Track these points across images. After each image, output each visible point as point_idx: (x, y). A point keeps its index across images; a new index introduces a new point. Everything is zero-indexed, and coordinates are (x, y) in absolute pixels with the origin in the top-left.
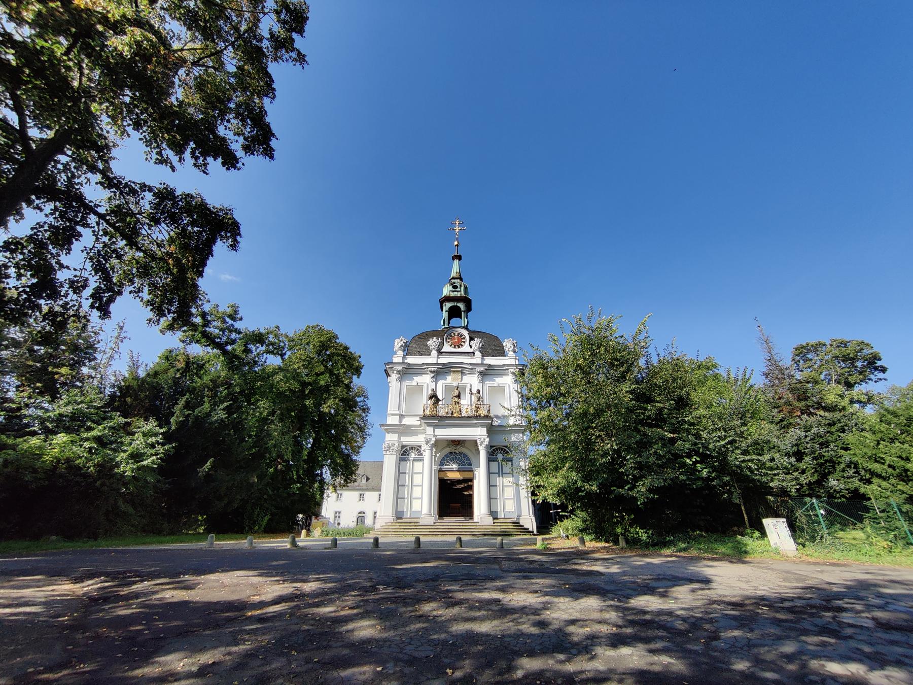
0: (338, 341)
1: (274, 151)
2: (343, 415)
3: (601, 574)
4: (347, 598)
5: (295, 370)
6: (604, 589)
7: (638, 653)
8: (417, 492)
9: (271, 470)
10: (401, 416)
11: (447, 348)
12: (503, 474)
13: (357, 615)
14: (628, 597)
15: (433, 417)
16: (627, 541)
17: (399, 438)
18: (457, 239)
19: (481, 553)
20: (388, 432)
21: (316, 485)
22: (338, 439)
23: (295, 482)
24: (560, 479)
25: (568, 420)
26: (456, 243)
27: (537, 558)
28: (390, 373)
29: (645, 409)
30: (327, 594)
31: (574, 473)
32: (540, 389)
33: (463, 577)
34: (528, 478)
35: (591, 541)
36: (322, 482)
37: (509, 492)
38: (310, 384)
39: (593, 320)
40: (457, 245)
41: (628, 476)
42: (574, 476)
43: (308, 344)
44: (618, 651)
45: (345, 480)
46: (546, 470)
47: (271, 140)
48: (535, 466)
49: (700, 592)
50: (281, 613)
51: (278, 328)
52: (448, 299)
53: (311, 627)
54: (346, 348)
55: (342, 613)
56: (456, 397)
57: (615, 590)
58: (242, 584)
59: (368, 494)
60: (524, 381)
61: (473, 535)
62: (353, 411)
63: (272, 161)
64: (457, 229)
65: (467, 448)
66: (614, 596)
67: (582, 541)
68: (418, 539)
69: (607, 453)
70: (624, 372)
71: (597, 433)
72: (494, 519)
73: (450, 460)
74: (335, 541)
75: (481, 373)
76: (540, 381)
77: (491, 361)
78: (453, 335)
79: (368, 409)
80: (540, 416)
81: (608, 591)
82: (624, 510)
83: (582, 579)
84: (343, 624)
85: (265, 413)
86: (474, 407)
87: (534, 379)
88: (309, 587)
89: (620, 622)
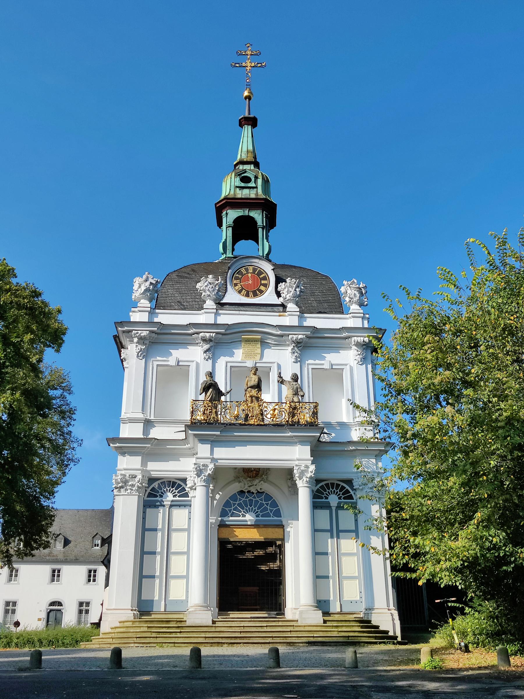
0: (14, 281)
10: (148, 424)
15: (208, 424)
17: (144, 463)
19: (321, 677)
20: (123, 454)
26: (246, 93)
28: (125, 340)
40: (249, 98)
45: (27, 544)
54: (36, 294)
59: (67, 570)
62: (45, 416)
67: (505, 656)
68: (196, 653)
74: (37, 657)
75: (298, 344)
78: (243, 270)
79: (72, 412)
86: (286, 407)
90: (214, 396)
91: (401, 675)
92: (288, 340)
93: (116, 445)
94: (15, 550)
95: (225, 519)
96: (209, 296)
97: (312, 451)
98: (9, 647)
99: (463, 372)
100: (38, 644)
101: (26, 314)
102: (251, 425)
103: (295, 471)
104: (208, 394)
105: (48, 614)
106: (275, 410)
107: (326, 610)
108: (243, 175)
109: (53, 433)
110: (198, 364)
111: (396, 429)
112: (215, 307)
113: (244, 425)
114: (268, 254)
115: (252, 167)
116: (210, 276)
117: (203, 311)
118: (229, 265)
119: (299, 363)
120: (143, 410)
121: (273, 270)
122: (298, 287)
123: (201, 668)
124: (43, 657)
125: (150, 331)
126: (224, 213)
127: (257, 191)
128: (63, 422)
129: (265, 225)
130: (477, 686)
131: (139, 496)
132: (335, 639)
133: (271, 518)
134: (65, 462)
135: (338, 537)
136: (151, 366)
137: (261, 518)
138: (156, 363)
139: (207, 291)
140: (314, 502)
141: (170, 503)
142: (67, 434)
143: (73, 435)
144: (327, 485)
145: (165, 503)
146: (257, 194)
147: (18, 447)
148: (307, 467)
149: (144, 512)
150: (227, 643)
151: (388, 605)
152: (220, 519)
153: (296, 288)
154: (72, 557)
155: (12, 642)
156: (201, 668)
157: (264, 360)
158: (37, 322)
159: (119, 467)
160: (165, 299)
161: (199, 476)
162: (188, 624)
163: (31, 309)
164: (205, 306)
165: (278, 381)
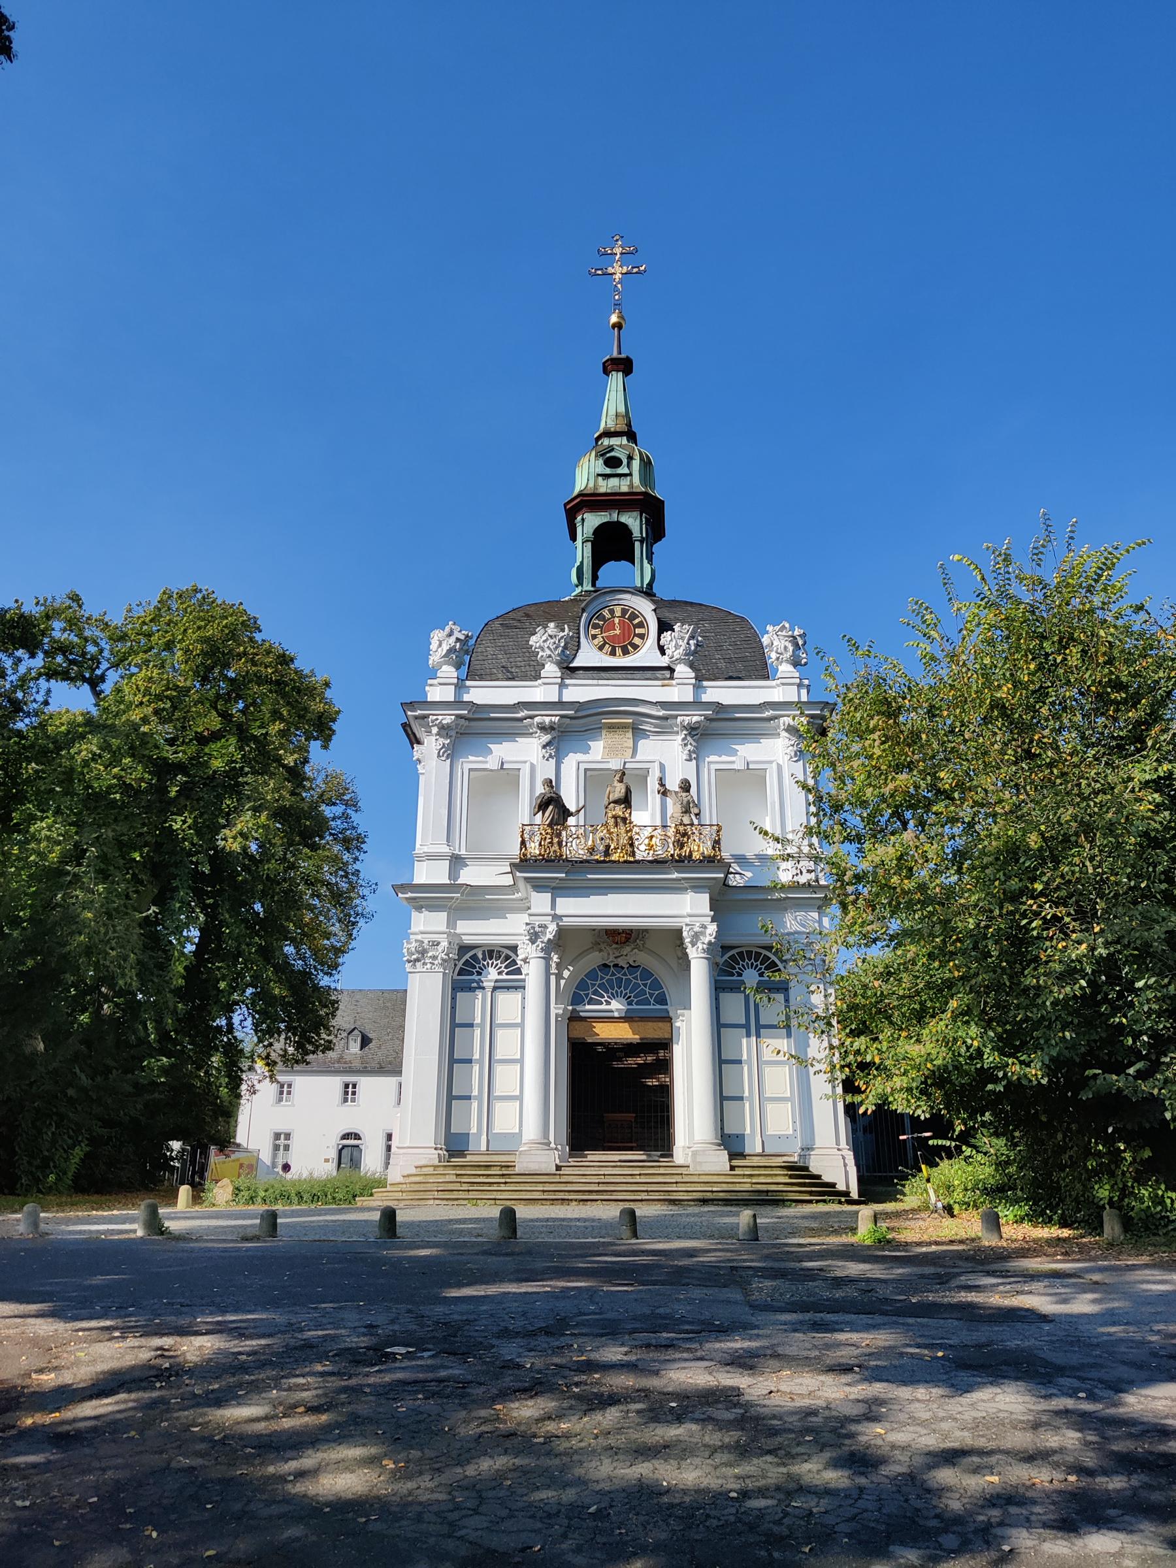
0: (258, 637)
1: (11, 28)
2: (284, 859)
3: (1044, 1318)
4: (301, 1380)
5: (135, 727)
6: (1046, 1364)
7: (1138, 1550)
9: (84, 1018)
10: (457, 862)
11: (589, 655)
12: (759, 1027)
13: (327, 1429)
14: (1119, 1387)
16: (1127, 1224)
17: (451, 923)
18: (617, 305)
19: (690, 1253)
20: (419, 909)
21: (216, 1060)
22: (272, 928)
23: (152, 1053)
24: (929, 1047)
25: (959, 871)
26: (614, 319)
27: (854, 1269)
28: (420, 732)
30: (243, 1368)
31: (974, 1030)
32: (875, 774)
33: (638, 1325)
34: (836, 1042)
35: (1020, 1221)
36: (233, 1052)
38: (180, 768)
39: (1048, 559)
40: (618, 326)
41: (1136, 1036)
42: (973, 1033)
43: (169, 646)
44: (1079, 1542)
45: (299, 1046)
46: (888, 1018)
48: (853, 1007)
50: (115, 1422)
51: (75, 598)
53: (199, 1461)
54: (285, 660)
55: (287, 1423)
56: (616, 802)
57: (1082, 1367)
58: (8, 1337)
59: (366, 1083)
60: (825, 755)
61: (673, 1202)
62: (314, 847)
64: (618, 271)
65: (652, 952)
66: (1076, 1383)
67: (993, 1222)
68: (509, 1216)
70: (1138, 723)
71: (1049, 911)
72: (732, 1156)
73: (601, 986)
75: (692, 730)
76: (877, 752)
78: (606, 613)
79: (360, 839)
80: (872, 857)
81: (1061, 1370)
82: (1121, 1134)
83: (984, 1333)
84: (289, 1454)
85: (53, 857)
86: (671, 832)
87: (856, 747)
89: (1090, 1460)
90: (556, 817)
91: (819, 1251)
92: (677, 726)
94: (280, 1055)
95: (579, 1008)
96: (550, 656)
97: (711, 899)
98: (253, 1203)
99: (341, 905)
101: (271, 692)
102: (614, 862)
103: (685, 934)
104: (547, 814)
105: (340, 1152)
106: (652, 837)
107: (739, 1150)
108: (608, 455)
109: (331, 874)
110: (533, 767)
111: (827, 868)
112: (559, 674)
113: (604, 862)
114: (650, 584)
115: (624, 440)
116: (552, 625)
117: (540, 681)
118: (583, 605)
119: (694, 761)
120: (448, 840)
121: (655, 610)
122: (692, 637)
123: (516, 1238)
124: (279, 1221)
125: (457, 716)
126: (579, 518)
127: (631, 481)
128: (346, 857)
129: (644, 535)
130: (987, 1268)
131: (444, 974)
132: (746, 1196)
133: (652, 1007)
134: (352, 919)
135: (758, 1036)
136: (460, 770)
137: (635, 1007)
138: (467, 767)
139: (547, 650)
140: (716, 981)
141: (492, 984)
142: (353, 874)
143: (362, 875)
144: (741, 954)
145: (485, 984)
147: (273, 897)
148: (704, 927)
149: (454, 999)
150: (576, 1200)
151: (838, 1143)
152: (570, 1008)
153: (689, 640)
156: (516, 1238)
157: (638, 757)
158: (288, 704)
159: (413, 929)
160: (482, 663)
161: (533, 943)
162: (517, 1170)
163: (278, 683)
165: (659, 792)
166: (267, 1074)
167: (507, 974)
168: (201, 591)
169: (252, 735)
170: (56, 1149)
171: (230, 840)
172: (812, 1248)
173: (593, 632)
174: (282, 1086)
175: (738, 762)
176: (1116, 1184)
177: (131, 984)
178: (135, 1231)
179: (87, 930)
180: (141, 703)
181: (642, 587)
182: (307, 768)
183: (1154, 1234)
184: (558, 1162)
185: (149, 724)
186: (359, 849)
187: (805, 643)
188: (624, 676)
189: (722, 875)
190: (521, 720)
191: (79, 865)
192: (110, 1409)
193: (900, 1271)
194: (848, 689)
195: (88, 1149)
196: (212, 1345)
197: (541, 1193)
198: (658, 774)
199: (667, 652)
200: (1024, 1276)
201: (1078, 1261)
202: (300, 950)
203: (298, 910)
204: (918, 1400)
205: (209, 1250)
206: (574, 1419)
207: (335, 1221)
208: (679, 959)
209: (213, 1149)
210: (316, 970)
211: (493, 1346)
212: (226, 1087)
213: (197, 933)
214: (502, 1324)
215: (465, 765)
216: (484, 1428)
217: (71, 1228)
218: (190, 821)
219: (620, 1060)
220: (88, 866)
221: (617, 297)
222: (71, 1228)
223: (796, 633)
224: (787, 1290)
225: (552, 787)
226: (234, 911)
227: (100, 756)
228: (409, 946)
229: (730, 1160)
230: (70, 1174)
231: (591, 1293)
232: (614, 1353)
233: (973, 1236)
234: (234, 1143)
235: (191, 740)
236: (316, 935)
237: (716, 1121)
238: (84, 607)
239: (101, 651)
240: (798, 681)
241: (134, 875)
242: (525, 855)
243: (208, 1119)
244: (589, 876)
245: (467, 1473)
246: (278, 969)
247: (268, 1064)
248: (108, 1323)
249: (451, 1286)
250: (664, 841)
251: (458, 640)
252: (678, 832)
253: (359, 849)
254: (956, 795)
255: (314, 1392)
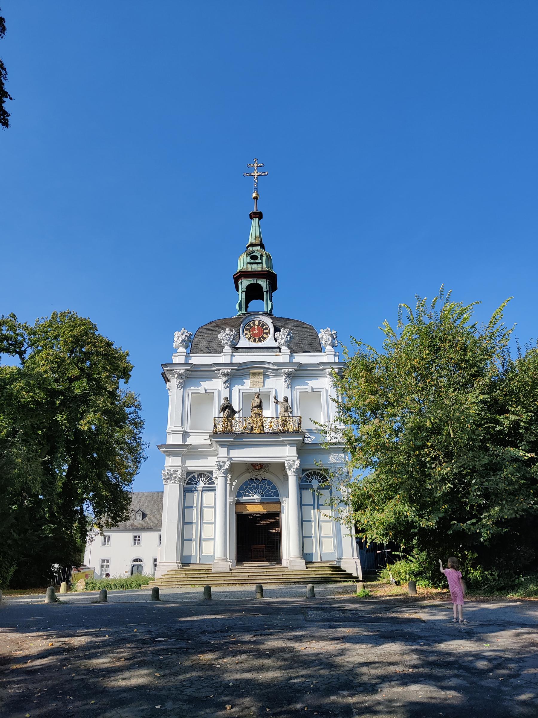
0: (96, 333)
1: (8, 116)
2: (108, 433)
3: (424, 622)
5: (41, 375)
8: (208, 531)
10: (186, 434)
11: (244, 342)
15: (226, 434)
17: (183, 462)
20: (169, 456)
21: (75, 525)
26: (254, 195)
28: (169, 377)
29: (497, 422)
30: (98, 647)
32: (362, 396)
33: (258, 628)
36: (83, 522)
37: (328, 528)
38: (61, 393)
40: (256, 198)
43: (56, 337)
45: (114, 518)
47: (4, 102)
49: (525, 636)
50: (50, 666)
51: (13, 316)
52: (244, 275)
53: (84, 677)
54: (109, 345)
55: (117, 664)
59: (144, 535)
62: (121, 427)
63: (6, 129)
64: (256, 174)
65: (272, 473)
67: (413, 586)
68: (208, 589)
69: (446, 479)
71: (433, 454)
72: (307, 563)
73: (250, 489)
75: (289, 375)
77: (302, 358)
78: (251, 324)
79: (142, 423)
82: (465, 548)
87: (355, 384)
88: (78, 641)
93: (163, 450)
94: (105, 523)
95: (240, 499)
97: (297, 449)
100: (113, 587)
102: (255, 433)
103: (286, 465)
105: (132, 568)
106: (271, 422)
107: (309, 560)
108: (252, 254)
109: (128, 439)
110: (219, 391)
112: (231, 351)
113: (250, 433)
114: (271, 310)
115: (259, 248)
116: (227, 329)
117: (222, 354)
118: (241, 321)
119: (290, 388)
121: (272, 322)
122: (288, 334)
125: (186, 370)
126: (240, 282)
127: (262, 266)
128: (135, 431)
130: (408, 604)
131: (180, 484)
133: (272, 497)
137: (265, 497)
138: (190, 392)
140: (300, 485)
142: (138, 439)
143: (142, 440)
145: (198, 489)
146: (262, 268)
147: (102, 450)
149: (184, 495)
151: (353, 556)
152: (236, 499)
153: (287, 336)
154: (148, 527)
155: (96, 587)
157: (265, 387)
158: (110, 364)
159: (166, 465)
160: (197, 345)
161: (219, 470)
162: (212, 571)
163: (106, 355)
164: (224, 351)
166: (99, 532)
167: (208, 484)
168: (71, 313)
169: (94, 378)
170: (2, 568)
171: (83, 425)
172: (337, 600)
173: (246, 332)
174: (105, 538)
175: (309, 388)
176: (464, 569)
177: (38, 491)
178: (44, 601)
179: (18, 467)
180: (44, 365)
181: (267, 312)
182: (118, 391)
183: (480, 590)
184: (231, 567)
185: (47, 374)
186: (141, 427)
187: (337, 337)
188: (259, 351)
189: (302, 439)
190: (214, 371)
191: (15, 437)
192: (46, 662)
193: (371, 606)
194: (352, 360)
195: (17, 568)
196: (85, 640)
197: (223, 581)
198: (274, 394)
199: (278, 341)
200: (421, 607)
201: (446, 601)
202: (114, 474)
203: (114, 456)
204: (362, 648)
205: (78, 607)
206: (229, 658)
207: (132, 595)
208: (284, 476)
209: (73, 568)
210: (121, 483)
211: (199, 637)
212: (80, 538)
213: (67, 467)
214: (203, 629)
215: (189, 391)
216: (194, 662)
217: (15, 601)
218: (65, 417)
219: (258, 521)
220: (19, 438)
221: (255, 186)
222: (15, 601)
223: (333, 333)
224: (321, 614)
225: (228, 401)
226: (84, 457)
227: (24, 388)
228: (164, 472)
229: (306, 564)
230: (8, 580)
231: (241, 618)
232: (248, 637)
233: (405, 593)
234: (83, 565)
235: (66, 380)
236: (122, 467)
237: (300, 547)
238: (17, 320)
239: (24, 339)
240: (334, 353)
241: (39, 441)
242: (216, 431)
243: (72, 553)
244: (244, 440)
245: (187, 677)
246: (104, 483)
247: (99, 527)
248: (40, 634)
249: (182, 617)
250: (277, 423)
251: (186, 336)
252: (282, 420)
253: (141, 427)
254: (395, 404)
255: (127, 654)
